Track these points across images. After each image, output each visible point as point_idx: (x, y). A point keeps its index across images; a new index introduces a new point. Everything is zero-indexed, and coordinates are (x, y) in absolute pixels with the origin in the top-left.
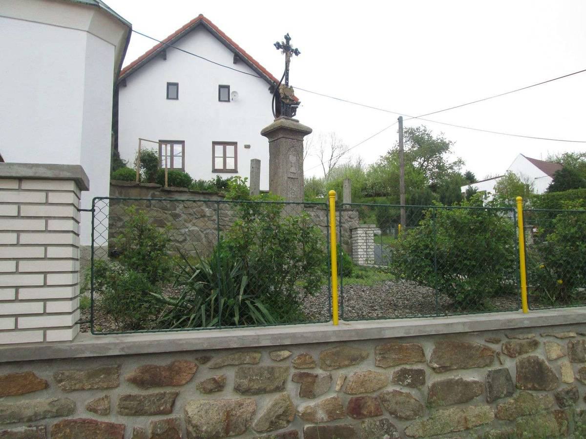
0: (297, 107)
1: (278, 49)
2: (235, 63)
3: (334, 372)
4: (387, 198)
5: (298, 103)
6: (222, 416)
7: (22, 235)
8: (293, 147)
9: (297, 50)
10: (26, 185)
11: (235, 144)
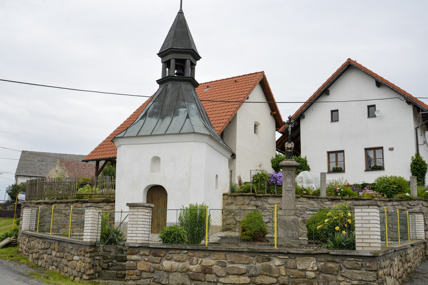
3: (198, 259)
6: (170, 266)
7: (363, 217)
8: (289, 174)
10: (135, 208)
11: (382, 148)
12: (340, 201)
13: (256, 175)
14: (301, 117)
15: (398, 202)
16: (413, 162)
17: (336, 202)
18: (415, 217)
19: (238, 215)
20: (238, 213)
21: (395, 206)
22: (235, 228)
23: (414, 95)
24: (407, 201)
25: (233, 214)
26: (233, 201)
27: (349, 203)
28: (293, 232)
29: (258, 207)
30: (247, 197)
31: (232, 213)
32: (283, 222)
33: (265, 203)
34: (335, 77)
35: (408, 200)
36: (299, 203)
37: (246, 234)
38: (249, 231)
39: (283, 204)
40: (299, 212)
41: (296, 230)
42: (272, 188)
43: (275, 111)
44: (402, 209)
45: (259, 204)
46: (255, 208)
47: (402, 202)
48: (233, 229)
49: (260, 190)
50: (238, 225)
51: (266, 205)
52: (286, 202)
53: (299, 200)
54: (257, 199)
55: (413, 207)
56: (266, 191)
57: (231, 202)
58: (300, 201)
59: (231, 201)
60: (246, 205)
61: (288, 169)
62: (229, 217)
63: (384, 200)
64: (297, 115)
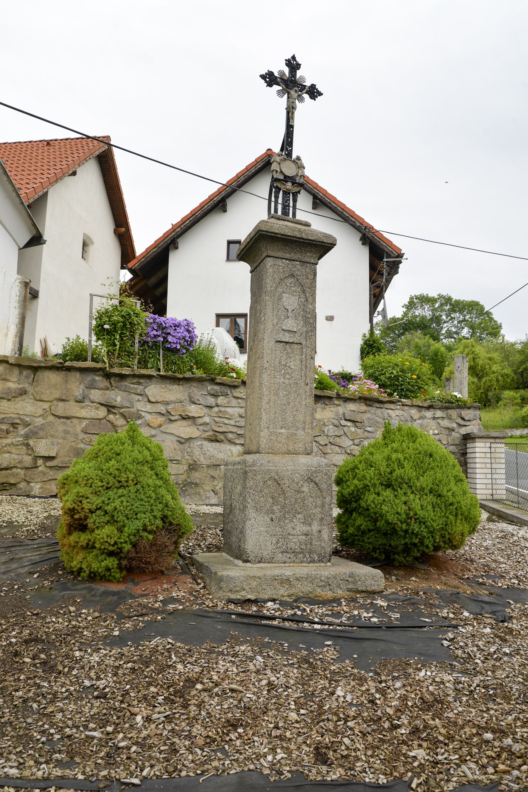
0: (400, 262)
1: (270, 85)
2: (314, 208)
4: (169, 565)
5: (400, 256)
8: (292, 276)
9: (313, 86)
12: (332, 402)
13: (107, 311)
14: (171, 247)
15: (443, 411)
16: (365, 343)
17: (323, 405)
18: (490, 447)
19: (41, 433)
20: (41, 429)
21: (439, 421)
22: (28, 482)
23: (377, 227)
24: (457, 410)
25: (22, 432)
26: (26, 386)
27: (352, 409)
28: (310, 525)
29: (114, 411)
30: (78, 374)
31: (20, 428)
32: (269, 483)
33: (138, 397)
34: (242, 179)
35: (459, 407)
36: (234, 402)
37: (89, 547)
38: (108, 530)
39: (265, 400)
40: (235, 430)
41: (322, 519)
42: (151, 356)
43: (122, 227)
44: (450, 427)
45: (119, 399)
46: (102, 412)
47: (449, 410)
48: (22, 485)
49: (119, 356)
50: (42, 472)
51: (139, 403)
52: (276, 394)
53: (235, 394)
54: (110, 383)
55: (468, 423)
56: (136, 362)
57: (20, 389)
58: (237, 398)
59: (20, 386)
60: (72, 403)
61: (288, 256)
62: (9, 441)
63: (421, 405)
64: (166, 240)
